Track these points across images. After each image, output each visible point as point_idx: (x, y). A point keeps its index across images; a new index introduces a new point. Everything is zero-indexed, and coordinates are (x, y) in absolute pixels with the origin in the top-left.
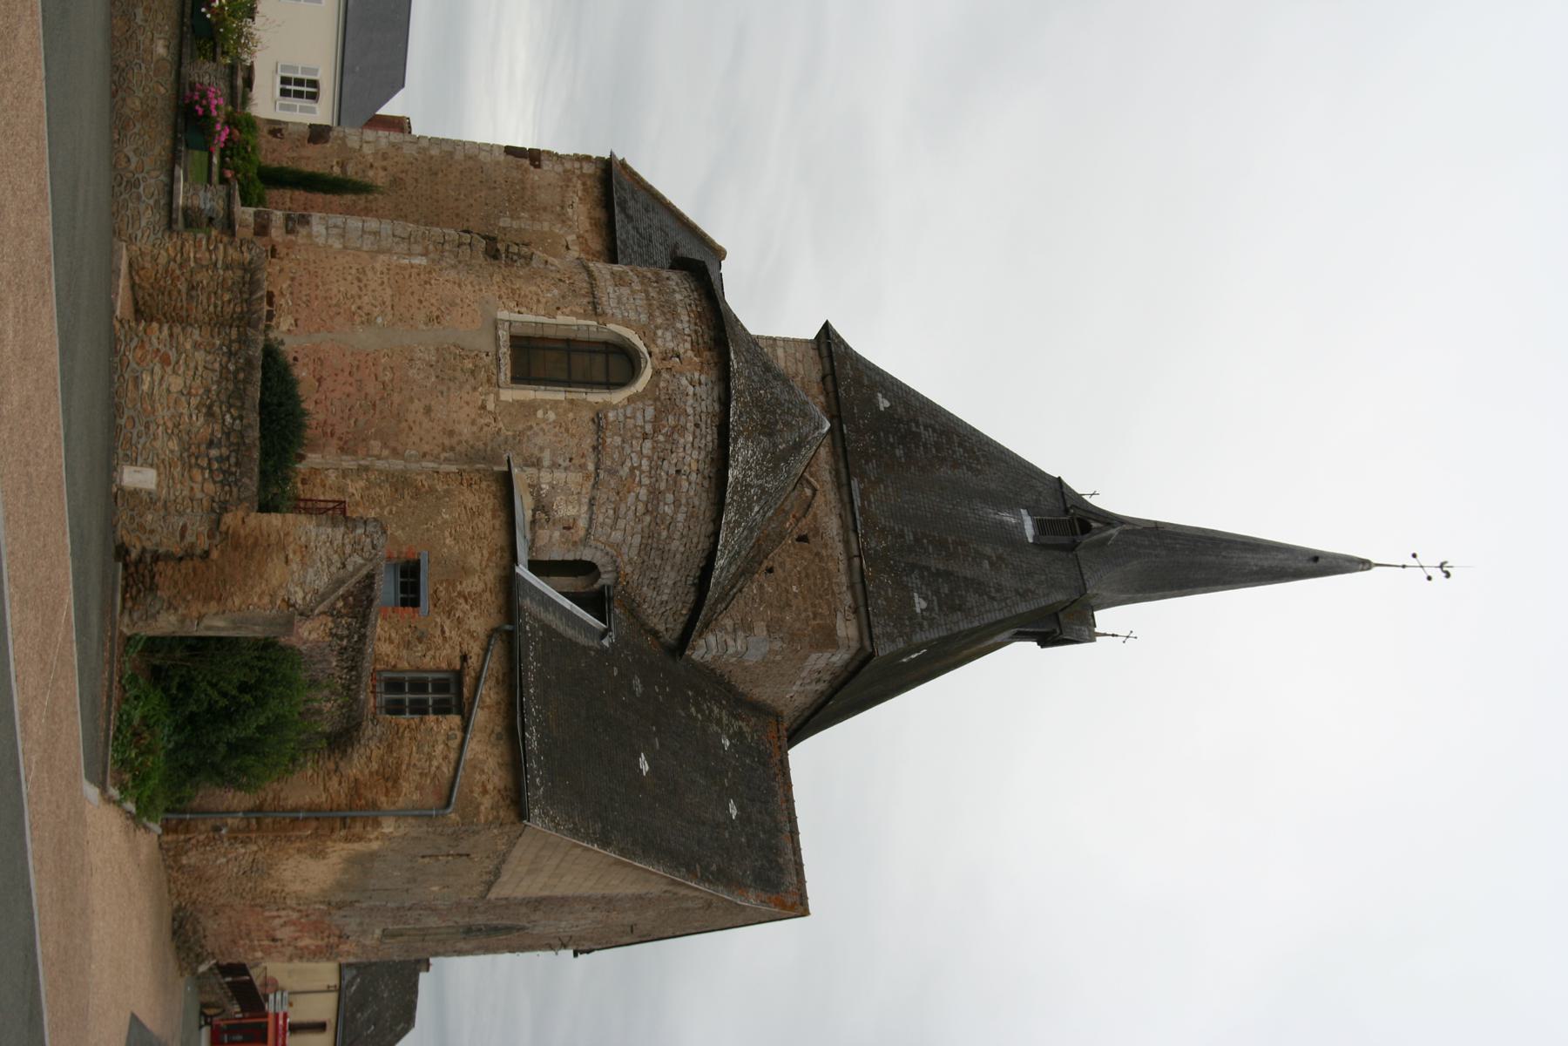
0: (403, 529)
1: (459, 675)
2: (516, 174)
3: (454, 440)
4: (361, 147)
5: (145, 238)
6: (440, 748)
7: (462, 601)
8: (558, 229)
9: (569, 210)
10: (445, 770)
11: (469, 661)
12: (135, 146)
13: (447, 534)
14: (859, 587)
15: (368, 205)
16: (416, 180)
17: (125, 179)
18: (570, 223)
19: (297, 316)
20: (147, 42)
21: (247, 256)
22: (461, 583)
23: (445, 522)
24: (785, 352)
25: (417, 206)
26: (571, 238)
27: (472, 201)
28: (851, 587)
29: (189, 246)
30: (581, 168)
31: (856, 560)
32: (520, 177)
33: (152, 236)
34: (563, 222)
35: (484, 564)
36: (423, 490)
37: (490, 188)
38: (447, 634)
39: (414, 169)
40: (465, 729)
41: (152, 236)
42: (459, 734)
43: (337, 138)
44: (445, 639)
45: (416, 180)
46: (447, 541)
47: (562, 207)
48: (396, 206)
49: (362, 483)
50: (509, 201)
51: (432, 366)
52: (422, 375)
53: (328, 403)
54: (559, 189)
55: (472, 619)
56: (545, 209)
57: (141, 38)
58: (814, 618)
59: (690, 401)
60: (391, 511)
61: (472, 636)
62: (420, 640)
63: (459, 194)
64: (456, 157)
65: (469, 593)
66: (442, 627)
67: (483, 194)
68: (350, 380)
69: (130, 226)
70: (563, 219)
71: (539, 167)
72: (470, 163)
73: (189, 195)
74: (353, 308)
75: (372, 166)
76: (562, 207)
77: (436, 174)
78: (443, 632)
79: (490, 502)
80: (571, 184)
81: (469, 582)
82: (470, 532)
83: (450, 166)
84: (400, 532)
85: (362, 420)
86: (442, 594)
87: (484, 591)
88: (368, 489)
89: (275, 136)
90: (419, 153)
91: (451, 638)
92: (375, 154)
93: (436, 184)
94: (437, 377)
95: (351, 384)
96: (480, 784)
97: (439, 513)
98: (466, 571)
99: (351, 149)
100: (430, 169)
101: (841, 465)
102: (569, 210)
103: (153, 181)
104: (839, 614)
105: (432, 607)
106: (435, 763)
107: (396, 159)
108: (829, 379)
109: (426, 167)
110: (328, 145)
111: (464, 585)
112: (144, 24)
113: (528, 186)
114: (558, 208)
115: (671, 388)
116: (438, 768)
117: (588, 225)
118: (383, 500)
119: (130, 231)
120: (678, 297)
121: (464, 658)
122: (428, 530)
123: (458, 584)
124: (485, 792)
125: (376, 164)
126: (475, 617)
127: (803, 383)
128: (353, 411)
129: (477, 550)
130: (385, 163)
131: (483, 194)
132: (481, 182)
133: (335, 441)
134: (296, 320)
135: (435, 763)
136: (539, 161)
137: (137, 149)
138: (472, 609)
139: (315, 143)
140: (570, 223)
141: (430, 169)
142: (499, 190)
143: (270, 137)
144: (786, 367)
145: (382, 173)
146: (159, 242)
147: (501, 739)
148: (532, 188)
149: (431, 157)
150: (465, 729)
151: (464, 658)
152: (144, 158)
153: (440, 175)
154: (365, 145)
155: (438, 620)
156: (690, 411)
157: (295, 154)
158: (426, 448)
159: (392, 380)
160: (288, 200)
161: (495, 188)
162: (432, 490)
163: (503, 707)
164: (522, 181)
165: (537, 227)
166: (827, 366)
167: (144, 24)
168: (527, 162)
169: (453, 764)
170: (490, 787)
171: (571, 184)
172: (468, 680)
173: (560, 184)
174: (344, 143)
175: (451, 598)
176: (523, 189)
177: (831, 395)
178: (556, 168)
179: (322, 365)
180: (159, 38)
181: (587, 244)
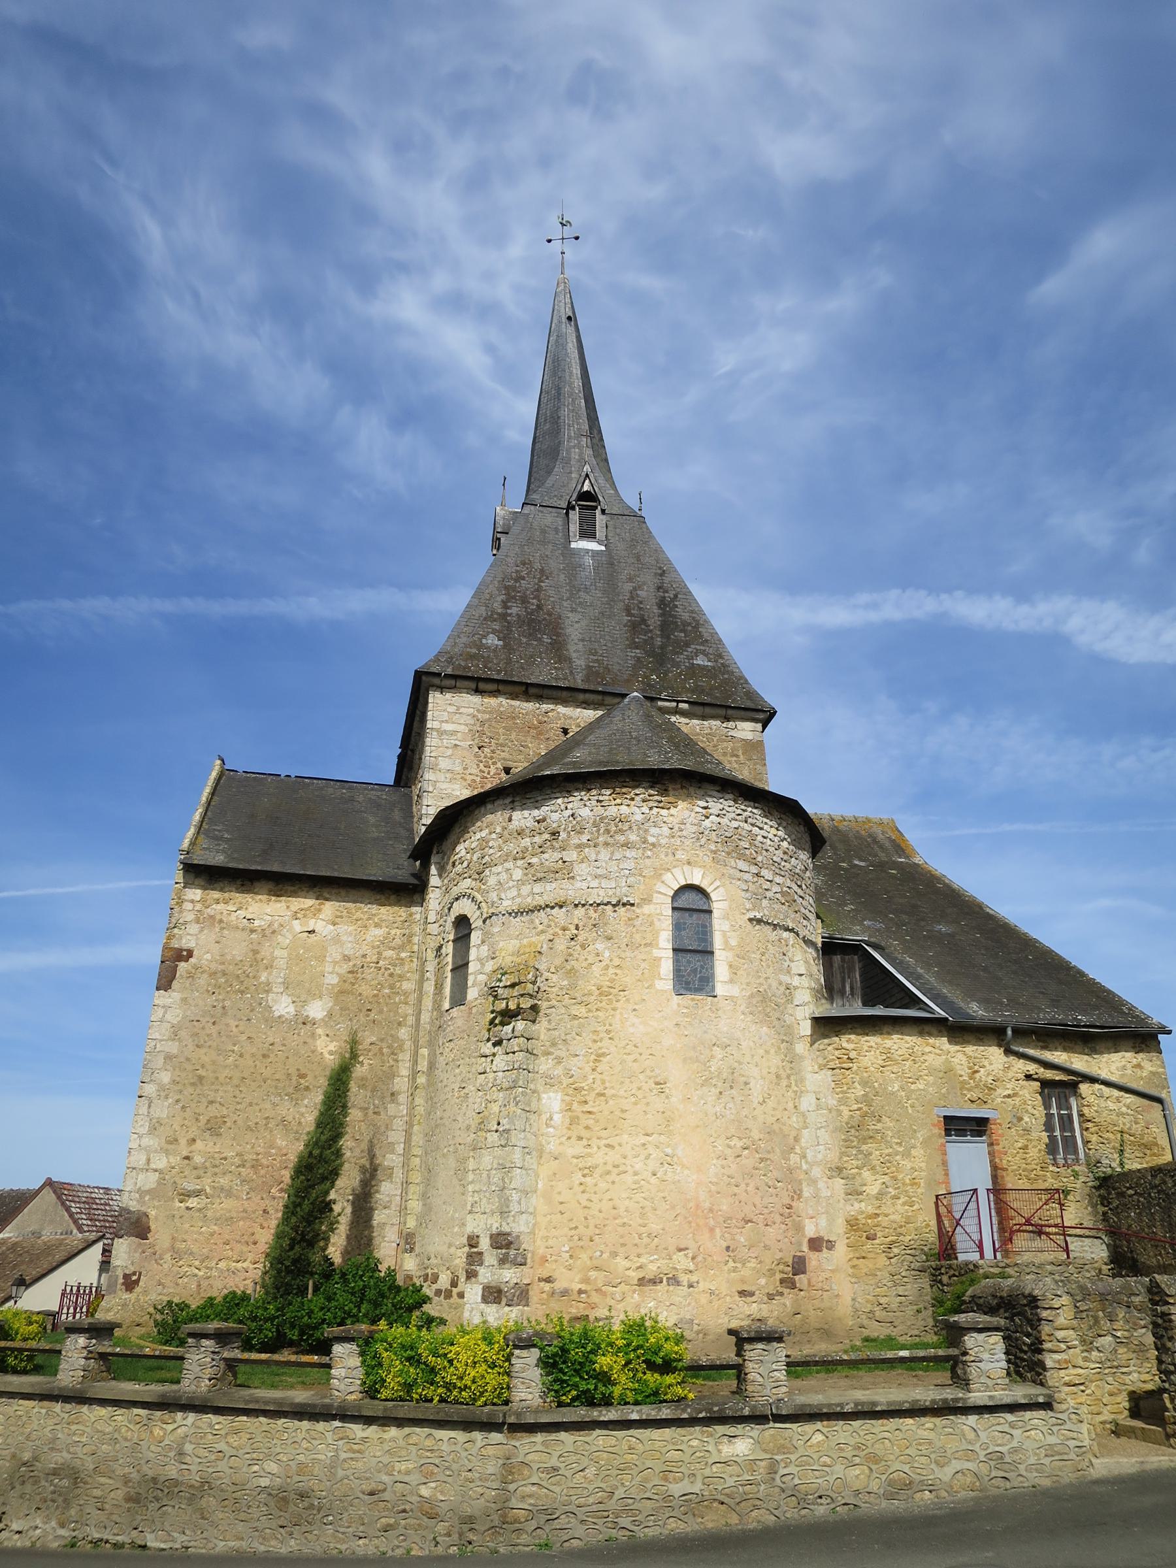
0: (915, 1131)
1: (1045, 1084)
2: (203, 980)
3: (784, 1075)
4: (156, 1171)
5: (1075, 1435)
6: (1112, 1106)
7: (977, 1076)
8: (285, 940)
9: (257, 923)
10: (1129, 1101)
11: (1031, 1073)
12: (933, 1466)
13: (913, 1087)
14: (708, 710)
15: (248, 1165)
16: (211, 1102)
17: (994, 1474)
18: (276, 925)
19: (672, 1249)
20: (734, 1469)
21: (1065, 1300)
22: (961, 1076)
23: (902, 1088)
24: (447, 722)
25: (251, 1104)
26: (297, 926)
27: (243, 1038)
28: (704, 718)
29: (1068, 1375)
30: (192, 901)
31: (681, 705)
32: (205, 976)
33: (1068, 1426)
34: (274, 932)
35: (938, 1051)
36: (865, 1109)
37: (225, 1014)
38: (1010, 1092)
39: (194, 1105)
40: (1093, 1080)
41: (1068, 1426)
42: (1097, 1086)
43: (141, 1200)
44: (1015, 1095)
45: (211, 1102)
46: (921, 1087)
47: (252, 931)
48: (249, 1128)
49: (866, 1174)
50: (242, 992)
51: (721, 1093)
52: (731, 1105)
53: (766, 1211)
54: (226, 932)
55: (992, 1067)
56: (255, 952)
57: (731, 1482)
58: (737, 756)
59: (724, 821)
60: (897, 1143)
61: (1008, 1068)
62: (1020, 1119)
63: (233, 1051)
64: (175, 1051)
65: (970, 1068)
66: (1005, 1097)
67: (233, 1023)
68: (743, 1186)
69: (1065, 1457)
70: (269, 933)
71: (190, 953)
72: (183, 1033)
73: (990, 1382)
74: (653, 1180)
75: (187, 1158)
76: (252, 931)
77: (201, 1078)
78: (1009, 1096)
79: (873, 1040)
80: (218, 917)
81: (958, 1067)
82: (908, 1063)
83: (188, 1059)
84: (919, 1135)
85: (776, 1174)
86: (974, 1095)
87: (964, 1053)
88: (873, 1168)
89: (137, 1282)
90: (167, 1097)
91: (1013, 1089)
92: (167, 1153)
93: (217, 1078)
94: (731, 1087)
95: (747, 1185)
96: (1134, 1070)
97: (893, 1093)
98: (949, 1071)
99: (159, 1183)
100: (193, 1084)
101: (581, 696)
102: (257, 923)
103: (983, 1435)
104: (730, 734)
105: (987, 1106)
106: (1124, 1109)
107: (176, 1127)
108: (482, 686)
109: (190, 1090)
110: (152, 1213)
111: (963, 1073)
112: (699, 1479)
113: (221, 967)
114: (253, 936)
115: (714, 838)
116: (1128, 1107)
117: (279, 905)
118: (887, 1151)
119: (1072, 1456)
120: (585, 812)
121: (1028, 1077)
122: (912, 1107)
123: (961, 1079)
124: (1138, 1066)
125: (185, 1153)
126: (991, 1064)
127: (484, 712)
128: (770, 1183)
129: (925, 1057)
130: (183, 1142)
131: (233, 1023)
132: (214, 1023)
133: (794, 1204)
134: (680, 1250)
135: (1124, 1109)
136: (182, 950)
137: (937, 1463)
138: (983, 1067)
139: (149, 1230)
140: (276, 925)
141: (193, 1084)
142: (227, 1003)
143: (138, 1290)
144: (466, 725)
145: (199, 1145)
146: (1073, 1416)
147: (1095, 1047)
148: (223, 963)
149: (174, 1082)
150: (1093, 1080)
151: (1028, 1077)
152: (949, 1452)
153: (201, 1072)
154: (153, 1166)
155: (999, 1100)
156: (735, 824)
157: (168, 1257)
158: (790, 1105)
159: (740, 1139)
160: (239, 1265)
161: (224, 1008)
162: (866, 1099)
163: (1066, 1044)
164: (213, 974)
165: (282, 963)
166: (466, 683)
167: (699, 1479)
168: (182, 966)
169: (1122, 1093)
170: (1135, 1061)
171: (218, 917)
172: (1050, 1075)
173: (217, 930)
174: (148, 1192)
175: (977, 1086)
176: (224, 974)
177: (501, 688)
178: (191, 932)
179: (730, 1218)
180: (719, 1451)
181: (306, 910)
